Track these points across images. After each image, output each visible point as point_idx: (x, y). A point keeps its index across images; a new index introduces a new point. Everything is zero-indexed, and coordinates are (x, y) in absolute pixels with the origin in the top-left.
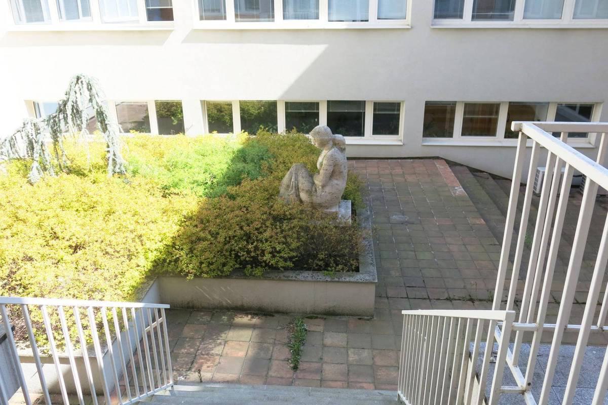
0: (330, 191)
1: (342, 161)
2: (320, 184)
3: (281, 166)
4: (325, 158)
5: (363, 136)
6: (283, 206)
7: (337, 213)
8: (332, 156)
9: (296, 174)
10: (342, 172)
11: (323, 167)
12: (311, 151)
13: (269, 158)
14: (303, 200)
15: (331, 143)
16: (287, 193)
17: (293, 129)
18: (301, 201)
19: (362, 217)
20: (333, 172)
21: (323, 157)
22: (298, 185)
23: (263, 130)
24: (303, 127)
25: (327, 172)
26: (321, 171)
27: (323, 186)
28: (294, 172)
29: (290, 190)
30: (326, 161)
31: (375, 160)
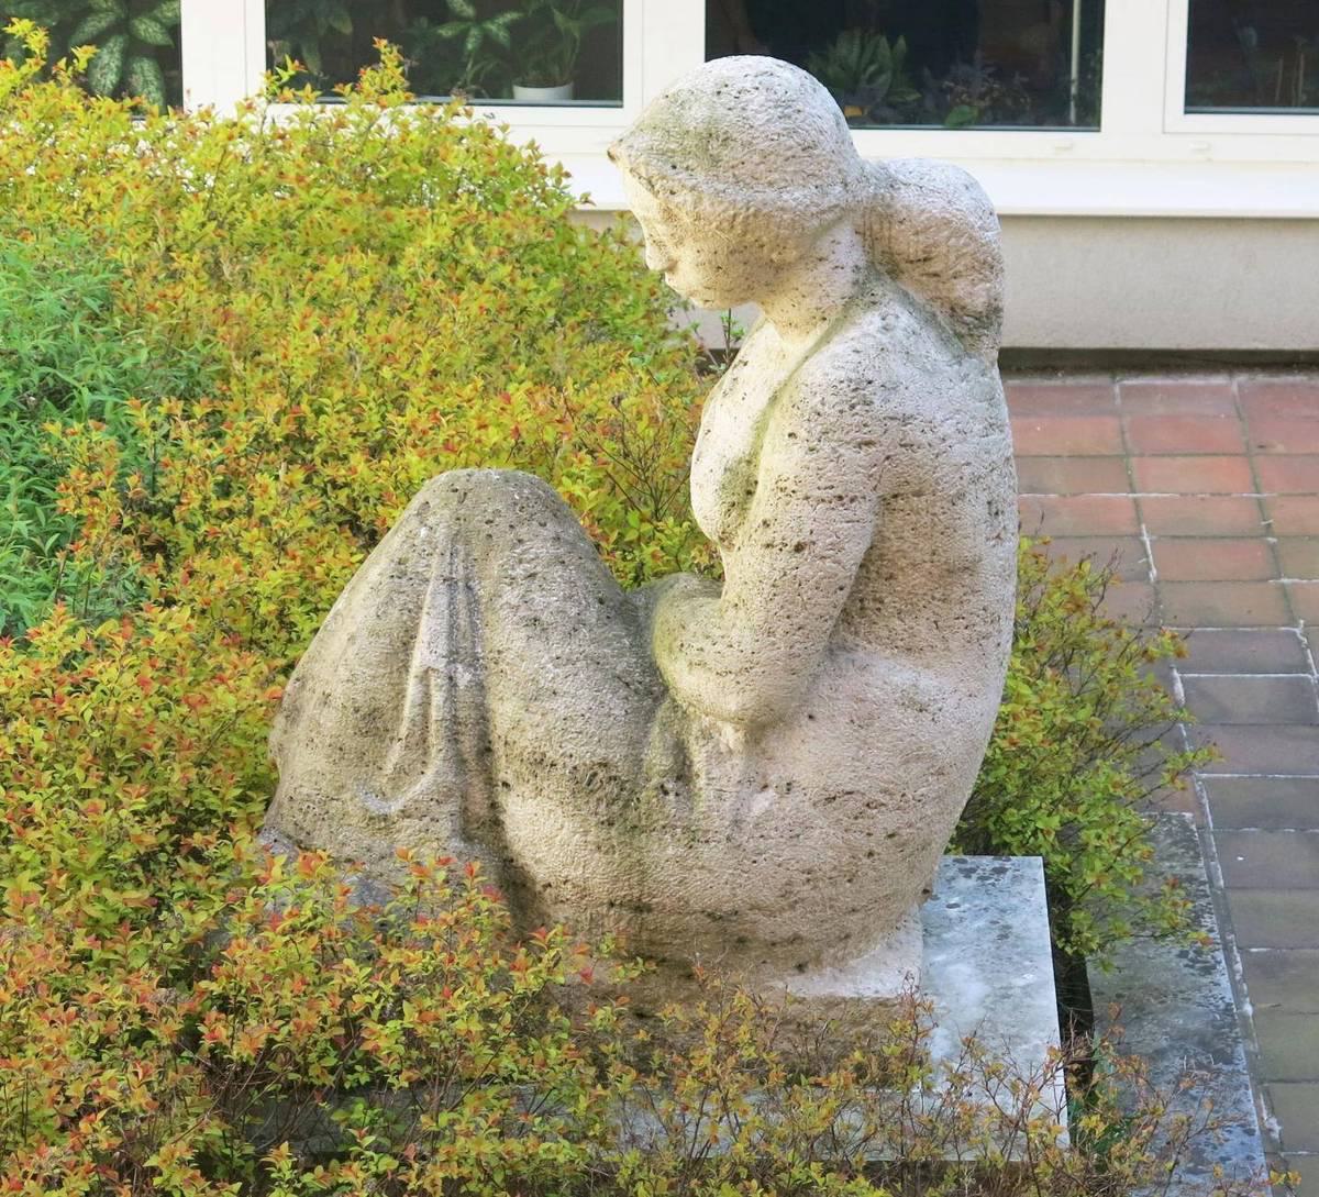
0: (843, 779)
1: (960, 451)
2: (732, 704)
3: (270, 486)
4: (781, 423)
5: (1088, 114)
6: (328, 958)
7: (912, 1012)
8: (858, 393)
9: (461, 587)
10: (969, 568)
11: (760, 507)
12: (566, 303)
13: (129, 385)
14: (540, 874)
15: (846, 250)
16: (354, 804)
17: (373, 59)
18: (515, 884)
19: (1152, 1035)
20: (873, 563)
21: (759, 400)
22: (483, 718)
23: (46, 74)
24: (446, 32)
25: (807, 567)
26: (744, 565)
27: (761, 728)
28: (436, 568)
29: (395, 753)
30: (798, 452)
31: (1218, 380)
